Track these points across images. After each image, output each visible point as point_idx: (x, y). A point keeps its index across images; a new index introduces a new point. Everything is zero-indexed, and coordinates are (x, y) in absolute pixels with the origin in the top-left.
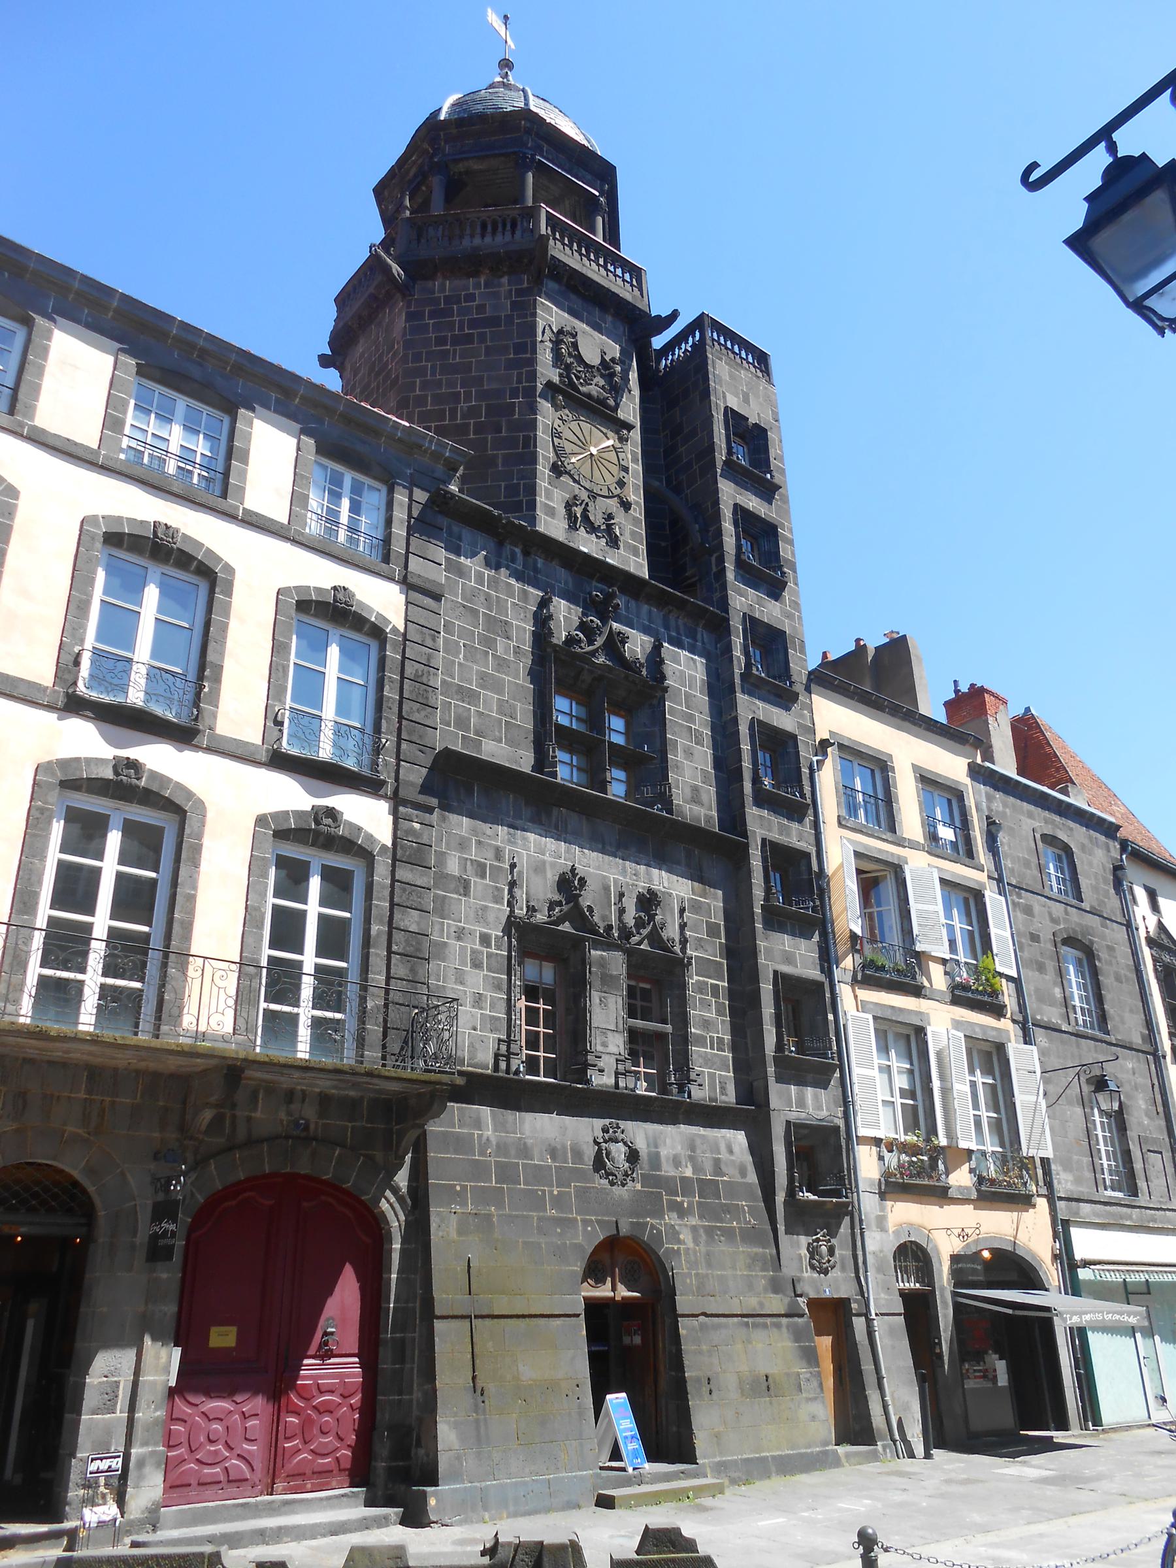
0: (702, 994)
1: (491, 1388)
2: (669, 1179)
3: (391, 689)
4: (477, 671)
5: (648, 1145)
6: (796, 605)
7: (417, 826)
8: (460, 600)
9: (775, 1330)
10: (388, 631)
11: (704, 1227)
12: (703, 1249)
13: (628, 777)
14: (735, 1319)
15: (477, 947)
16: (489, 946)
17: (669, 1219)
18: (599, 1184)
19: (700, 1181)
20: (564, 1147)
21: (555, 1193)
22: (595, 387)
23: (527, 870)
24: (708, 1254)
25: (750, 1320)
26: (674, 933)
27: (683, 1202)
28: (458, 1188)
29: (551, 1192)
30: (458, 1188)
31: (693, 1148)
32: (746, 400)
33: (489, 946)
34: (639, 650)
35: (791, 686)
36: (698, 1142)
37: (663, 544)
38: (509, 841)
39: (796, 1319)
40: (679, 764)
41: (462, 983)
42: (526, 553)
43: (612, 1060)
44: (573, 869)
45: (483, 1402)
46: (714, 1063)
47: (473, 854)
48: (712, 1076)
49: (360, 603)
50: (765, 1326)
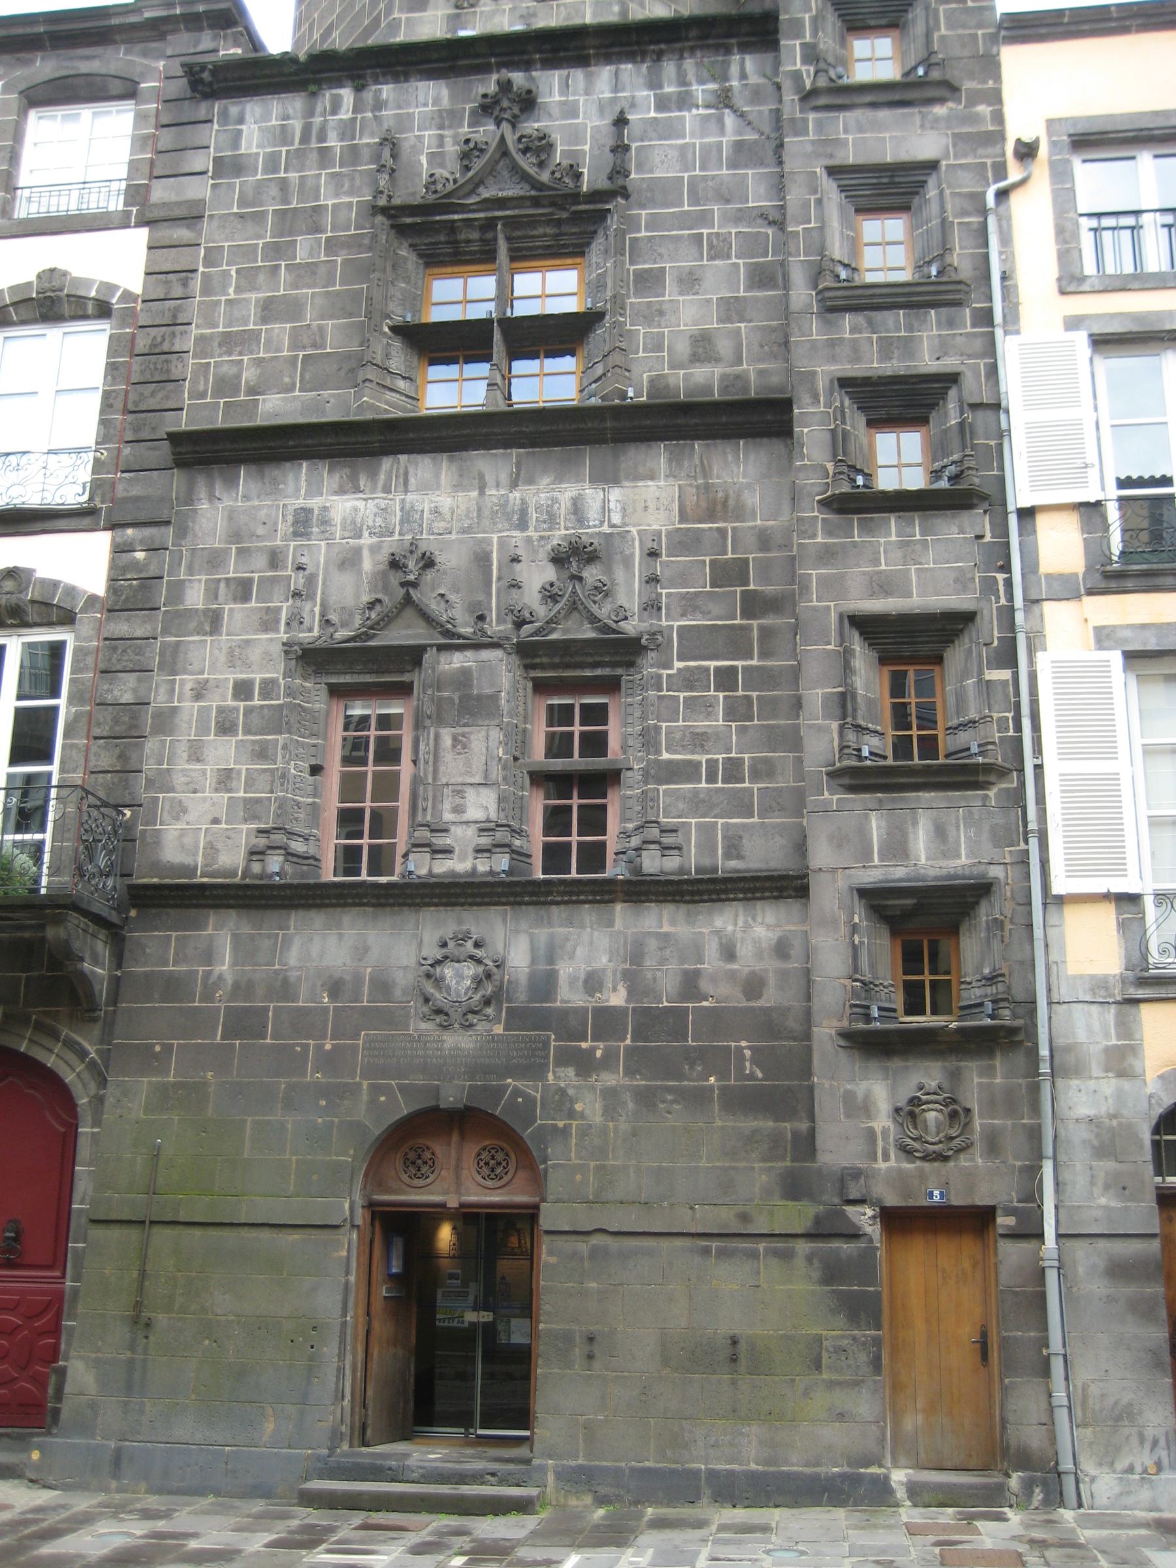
0: (692, 689)
1: (162, 1319)
5: (534, 961)
7: (140, 555)
9: (774, 1262)
10: (114, 301)
12: (624, 1126)
14: (678, 1243)
17: (556, 1078)
18: (416, 1030)
20: (358, 979)
23: (326, 569)
25: (714, 1245)
27: (593, 1050)
28: (158, 1048)
29: (320, 1048)
30: (158, 1048)
31: (637, 955)
36: (652, 944)
38: (296, 534)
39: (835, 1244)
40: (665, 307)
41: (198, 760)
43: (471, 831)
45: (146, 1337)
47: (232, 570)
48: (707, 832)
50: (754, 1255)
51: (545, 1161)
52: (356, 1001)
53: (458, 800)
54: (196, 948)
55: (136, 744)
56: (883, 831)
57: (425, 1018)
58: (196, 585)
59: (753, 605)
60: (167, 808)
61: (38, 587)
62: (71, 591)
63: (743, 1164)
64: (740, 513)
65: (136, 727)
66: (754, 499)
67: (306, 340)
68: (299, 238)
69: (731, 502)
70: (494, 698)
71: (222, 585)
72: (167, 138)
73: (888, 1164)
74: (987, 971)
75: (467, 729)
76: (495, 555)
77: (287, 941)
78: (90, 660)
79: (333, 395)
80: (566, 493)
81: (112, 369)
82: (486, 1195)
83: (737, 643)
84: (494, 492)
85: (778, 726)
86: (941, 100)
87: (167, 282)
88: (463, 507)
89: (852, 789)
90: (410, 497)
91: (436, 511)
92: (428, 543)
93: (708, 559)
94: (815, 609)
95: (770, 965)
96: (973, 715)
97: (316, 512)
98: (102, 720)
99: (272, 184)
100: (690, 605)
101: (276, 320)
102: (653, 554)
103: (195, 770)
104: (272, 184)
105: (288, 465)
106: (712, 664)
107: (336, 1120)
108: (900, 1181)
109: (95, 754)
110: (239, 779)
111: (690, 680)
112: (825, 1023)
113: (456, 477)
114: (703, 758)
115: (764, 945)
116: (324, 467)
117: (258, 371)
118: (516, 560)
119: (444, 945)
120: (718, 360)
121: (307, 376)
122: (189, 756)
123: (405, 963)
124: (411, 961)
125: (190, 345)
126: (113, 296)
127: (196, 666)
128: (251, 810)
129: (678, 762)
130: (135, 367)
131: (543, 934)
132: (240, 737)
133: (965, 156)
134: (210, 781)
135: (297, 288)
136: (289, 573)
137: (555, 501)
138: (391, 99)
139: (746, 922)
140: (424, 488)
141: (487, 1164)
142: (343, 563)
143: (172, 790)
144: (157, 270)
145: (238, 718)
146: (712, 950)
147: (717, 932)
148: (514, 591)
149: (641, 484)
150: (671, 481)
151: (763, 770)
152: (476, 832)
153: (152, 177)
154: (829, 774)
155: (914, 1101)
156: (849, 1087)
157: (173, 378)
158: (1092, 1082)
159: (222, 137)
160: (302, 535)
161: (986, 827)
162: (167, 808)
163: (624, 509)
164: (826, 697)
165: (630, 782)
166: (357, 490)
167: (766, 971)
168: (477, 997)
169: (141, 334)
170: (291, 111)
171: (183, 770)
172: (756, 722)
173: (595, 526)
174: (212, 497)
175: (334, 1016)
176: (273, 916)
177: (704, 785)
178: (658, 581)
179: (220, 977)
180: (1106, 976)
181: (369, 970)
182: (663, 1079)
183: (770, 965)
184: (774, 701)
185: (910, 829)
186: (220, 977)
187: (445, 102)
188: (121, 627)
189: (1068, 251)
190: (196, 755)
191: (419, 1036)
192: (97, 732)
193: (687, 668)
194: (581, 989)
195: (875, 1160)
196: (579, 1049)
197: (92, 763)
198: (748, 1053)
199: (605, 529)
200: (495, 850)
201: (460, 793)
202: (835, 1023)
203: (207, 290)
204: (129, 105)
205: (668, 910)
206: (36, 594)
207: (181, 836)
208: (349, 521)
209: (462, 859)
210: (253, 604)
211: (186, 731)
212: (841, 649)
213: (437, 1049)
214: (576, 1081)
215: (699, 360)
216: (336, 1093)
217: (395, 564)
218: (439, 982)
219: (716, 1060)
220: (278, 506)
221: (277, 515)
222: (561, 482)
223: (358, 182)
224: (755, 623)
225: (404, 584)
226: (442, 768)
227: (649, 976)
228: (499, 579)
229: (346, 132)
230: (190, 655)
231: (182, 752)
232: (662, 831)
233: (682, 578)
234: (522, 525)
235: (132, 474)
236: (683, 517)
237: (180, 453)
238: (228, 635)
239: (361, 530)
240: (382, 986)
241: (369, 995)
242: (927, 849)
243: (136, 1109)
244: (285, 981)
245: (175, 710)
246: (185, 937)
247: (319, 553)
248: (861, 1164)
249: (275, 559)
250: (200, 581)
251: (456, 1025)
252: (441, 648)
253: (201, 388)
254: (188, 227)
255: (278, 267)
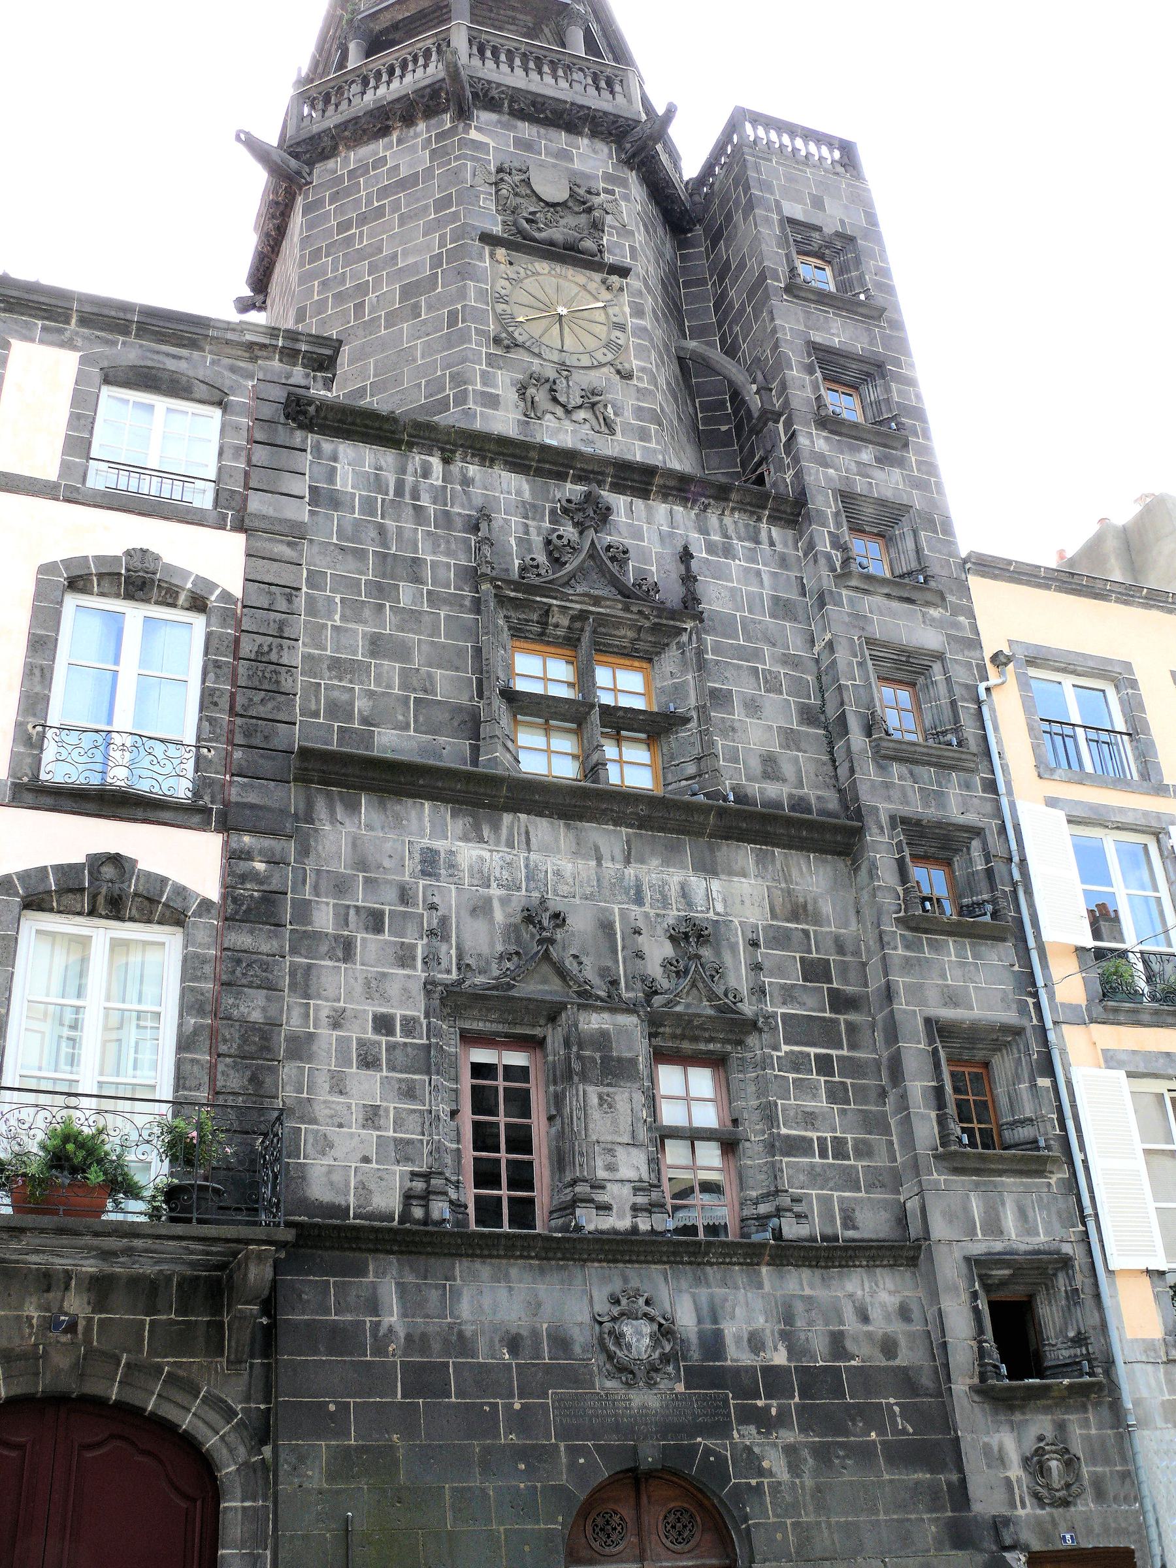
0: (798, 1071)
2: (737, 1371)
3: (217, 676)
4: (364, 634)
5: (700, 1321)
6: (930, 468)
7: (260, 866)
8: (335, 541)
11: (806, 1445)
12: (809, 1482)
13: (653, 757)
15: (370, 1035)
16: (390, 1032)
17: (742, 1436)
18: (603, 1389)
19: (803, 1371)
20: (535, 1334)
21: (517, 1406)
22: (560, 230)
23: (458, 913)
24: (818, 1489)
26: (739, 977)
27: (767, 1408)
28: (332, 1407)
31: (788, 1318)
32: (818, 203)
33: (390, 1032)
34: (654, 569)
35: (926, 581)
36: (799, 1307)
37: (724, 428)
38: (424, 873)
40: (736, 725)
42: (446, 461)
43: (627, 1190)
44: (543, 901)
46: (827, 1180)
47: (360, 898)
48: (826, 1201)
49: (168, 567)
51: (746, 1519)
52: (538, 1358)
53: (609, 1158)
54: (358, 1297)
55: (270, 1068)
56: (982, 1210)
57: (610, 1376)
58: (323, 907)
59: (841, 1002)
60: (311, 1140)
61: (142, 881)
62: (181, 891)
63: (913, 1516)
64: (817, 920)
65: (268, 1049)
66: (827, 908)
67: (415, 683)
68: (401, 584)
69: (810, 907)
70: (633, 1062)
71: (352, 912)
72: (261, 455)
73: (1026, 1511)
74: (1071, 1334)
75: (611, 1090)
76: (618, 924)
77: (456, 1294)
78: (208, 969)
79: (449, 743)
80: (675, 877)
81: (210, 667)
82: (676, 1560)
83: (826, 1033)
84: (610, 865)
85: (871, 1112)
86: (934, 605)
87: (270, 593)
88: (584, 874)
89: (957, 1171)
90: (533, 856)
91: (558, 873)
92: (556, 904)
93: (798, 955)
94: (905, 1011)
95: (897, 1328)
96: (1028, 1114)
97: (443, 855)
98: (228, 1037)
99: (370, 526)
100: (788, 996)
101: (384, 657)
102: (754, 944)
103: (339, 1103)
104: (371, 527)
105: (410, 801)
106: (813, 1051)
107: (539, 1485)
108: (1039, 1527)
109: (223, 1073)
110: (387, 1117)
111: (797, 1063)
112: (960, 1380)
113: (574, 845)
114: (814, 1135)
115: (890, 1309)
116: (446, 811)
117: (371, 703)
118: (637, 932)
119: (617, 1302)
120: (784, 780)
121: (421, 719)
122: (331, 1088)
123: (580, 1319)
124: (586, 1318)
125: (298, 661)
126: (212, 594)
127: (331, 992)
128: (403, 1150)
129: (795, 1138)
130: (241, 670)
131: (703, 1293)
132: (385, 1073)
133: (957, 654)
134: (356, 1116)
135: (403, 631)
136: (421, 911)
137: (665, 883)
138: (477, 479)
139: (871, 1287)
140: (546, 850)
141: (673, 1527)
142: (474, 910)
143: (313, 1121)
144: (259, 579)
145: (380, 1053)
146: (849, 1314)
147: (850, 1296)
148: (638, 961)
149: (736, 879)
150: (760, 880)
151: (864, 1150)
152: (631, 1191)
153: (247, 487)
154: (935, 1157)
155: (1039, 1452)
156: (986, 1440)
157: (282, 690)
158: (1158, 1433)
159: (316, 468)
160: (430, 875)
161: (1054, 1209)
162: (311, 1140)
163: (725, 901)
164: (924, 1088)
165: (749, 1153)
166: (481, 840)
167: (896, 1332)
168: (656, 1355)
169: (245, 638)
170: (383, 463)
171: (325, 1102)
172: (852, 1106)
173: (702, 912)
174: (333, 820)
175: (519, 1374)
176: (436, 1264)
177: (817, 1160)
178: (761, 969)
179: (390, 1329)
180: (1153, 1340)
181: (545, 1326)
182: (833, 1436)
183: (897, 1328)
184: (864, 1088)
185: (1000, 1208)
186: (390, 1329)
187: (527, 495)
188: (242, 939)
189: (1039, 745)
190: (339, 1086)
191: (606, 1395)
192: (223, 1048)
193: (792, 1052)
194: (747, 1348)
195: (1016, 1508)
196: (756, 1405)
197: (219, 1084)
198: (897, 1409)
199: (711, 915)
200: (654, 1210)
201: (611, 1151)
202: (968, 1381)
203: (312, 610)
204: (217, 413)
205: (806, 1273)
206: (141, 888)
207: (329, 1172)
208: (476, 870)
209: (621, 1216)
210: (386, 936)
211: (325, 1059)
212: (930, 1049)
213: (626, 1408)
214: (759, 1439)
215: (769, 778)
216: (536, 1456)
217: (529, 918)
218: (618, 1338)
219: (873, 1416)
220: (403, 842)
221: (404, 851)
222: (668, 866)
223: (453, 546)
224: (842, 1017)
225: (541, 942)
226: (591, 1126)
227: (803, 1337)
228: (623, 948)
229: (439, 496)
230: (323, 979)
231: (323, 1082)
232: (792, 1201)
233: (780, 971)
234: (639, 900)
235: (245, 780)
236: (774, 916)
237: (306, 769)
238: (363, 964)
239: (489, 880)
240: (561, 1343)
241: (550, 1352)
242: (1016, 1227)
243: (315, 1477)
244: (461, 1335)
245: (311, 1037)
246: (344, 1283)
247: (451, 899)
248: (1005, 1511)
249: (405, 895)
250: (327, 904)
251: (641, 1384)
252: (581, 1007)
253: (313, 707)
254: (289, 544)
255: (382, 606)
